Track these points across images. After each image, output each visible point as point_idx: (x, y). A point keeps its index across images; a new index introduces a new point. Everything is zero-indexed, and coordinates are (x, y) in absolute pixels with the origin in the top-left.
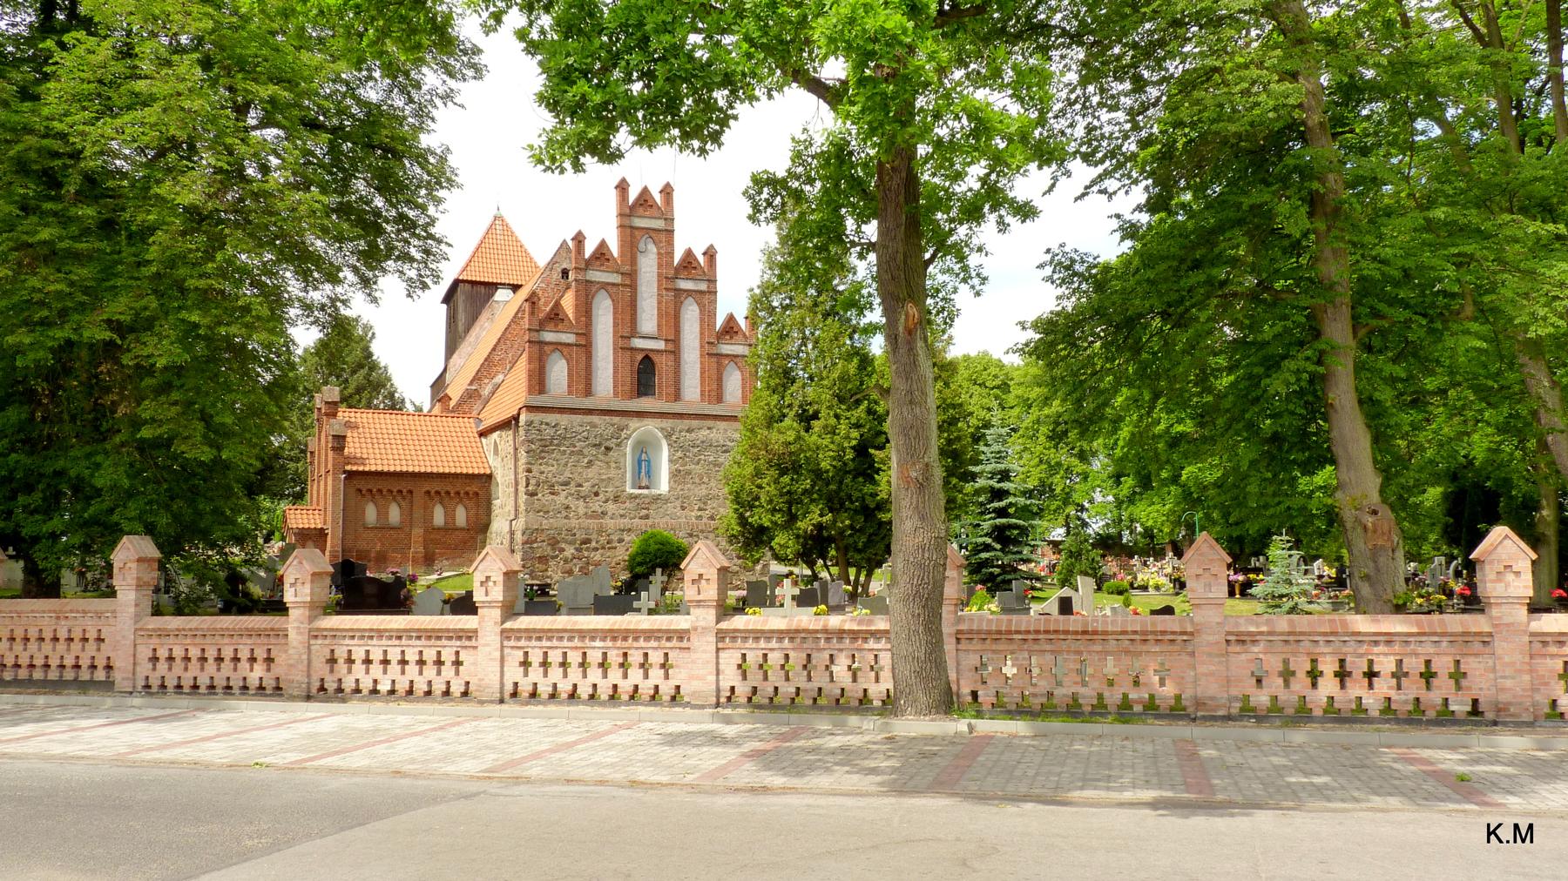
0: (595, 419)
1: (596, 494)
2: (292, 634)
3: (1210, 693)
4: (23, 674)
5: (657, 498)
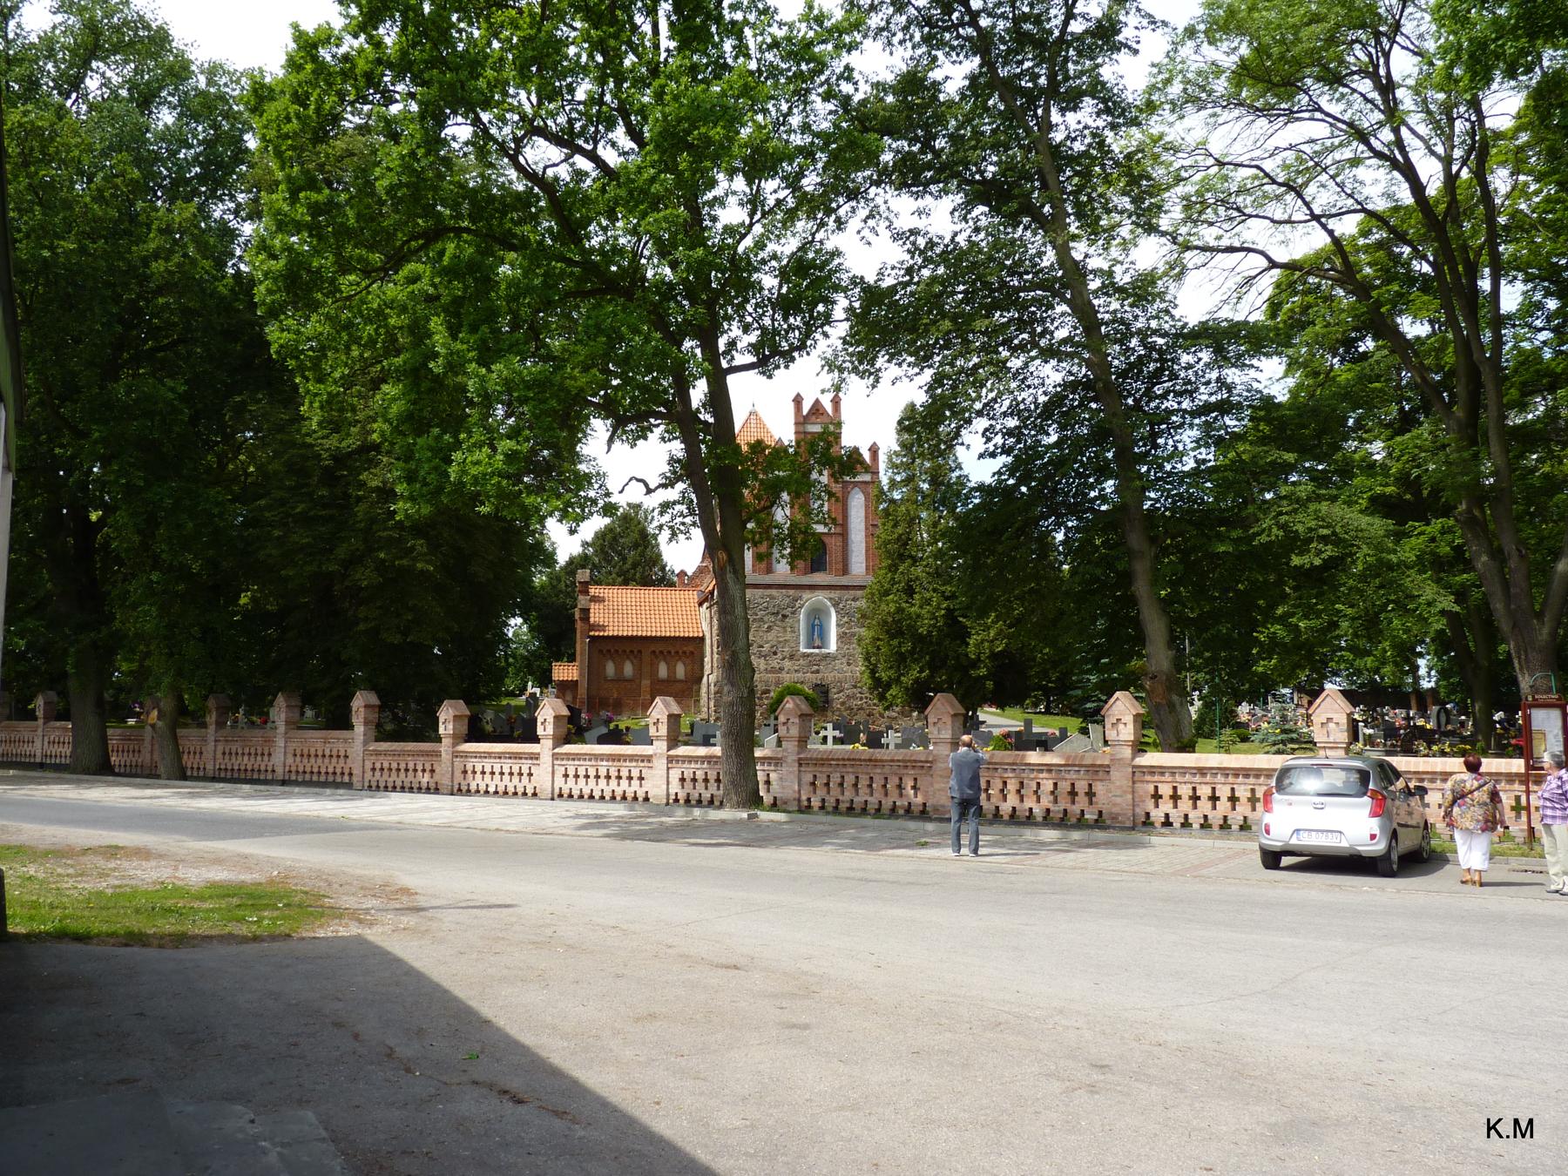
0: (774, 592)
1: (775, 653)
2: (443, 754)
3: (942, 802)
4: (307, 777)
5: (827, 656)
